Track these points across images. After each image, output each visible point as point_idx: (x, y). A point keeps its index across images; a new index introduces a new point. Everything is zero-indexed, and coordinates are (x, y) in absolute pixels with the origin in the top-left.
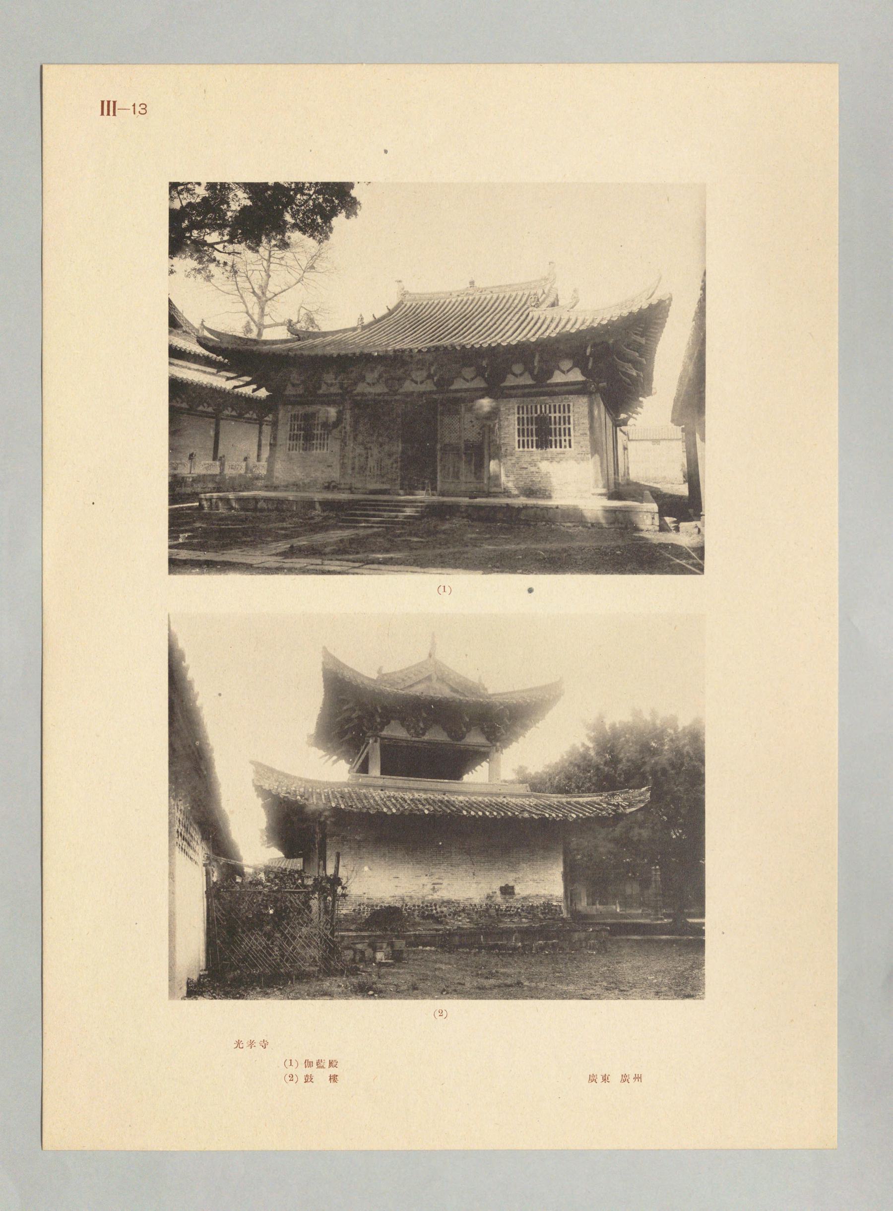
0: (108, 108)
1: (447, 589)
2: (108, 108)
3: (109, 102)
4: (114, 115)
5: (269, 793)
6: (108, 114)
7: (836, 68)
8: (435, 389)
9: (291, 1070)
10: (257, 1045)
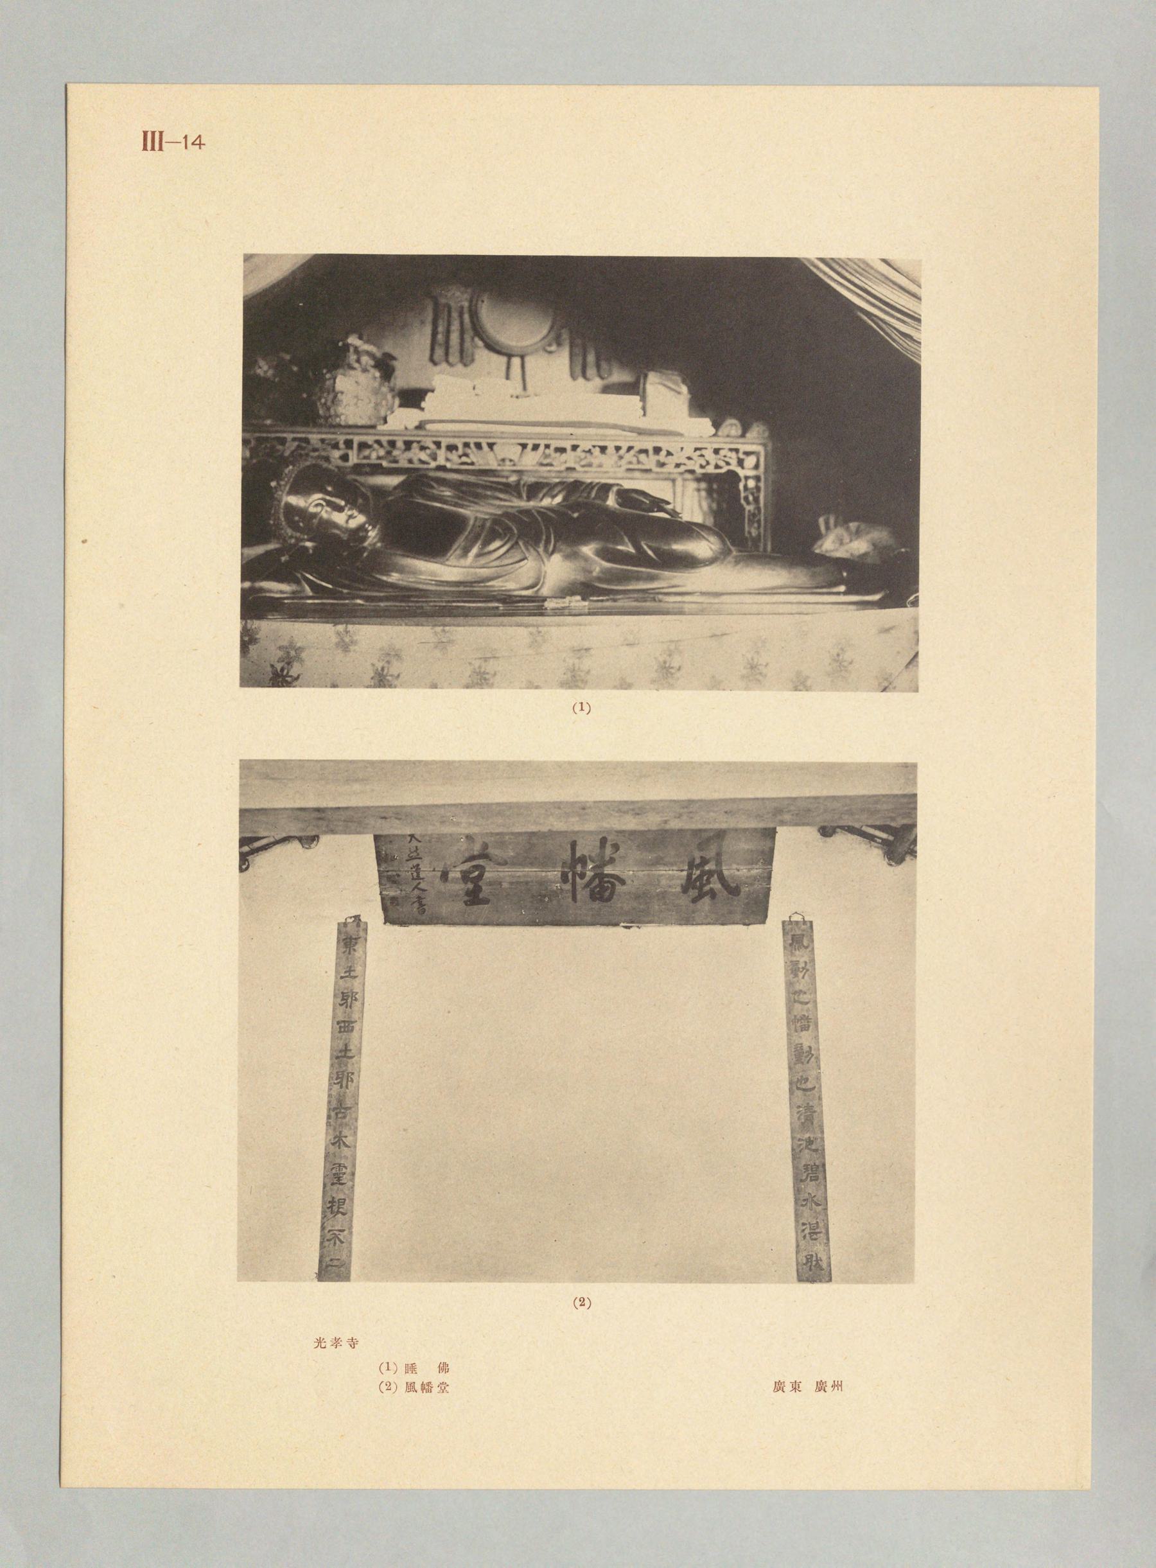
0: (152, 141)
2: (152, 141)
3: (153, 149)
4: (161, 149)
5: (706, 478)
6: (153, 149)
8: (578, 855)
9: (388, 1376)
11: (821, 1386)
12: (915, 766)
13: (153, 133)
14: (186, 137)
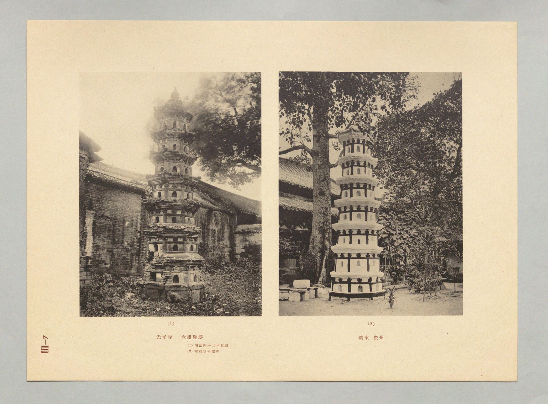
0: (45, 350)
1: (172, 323)
2: (45, 350)
4: (48, 347)
6: (42, 349)
7: (30, 22)
10: (167, 337)
11: (376, 338)
13: (42, 349)
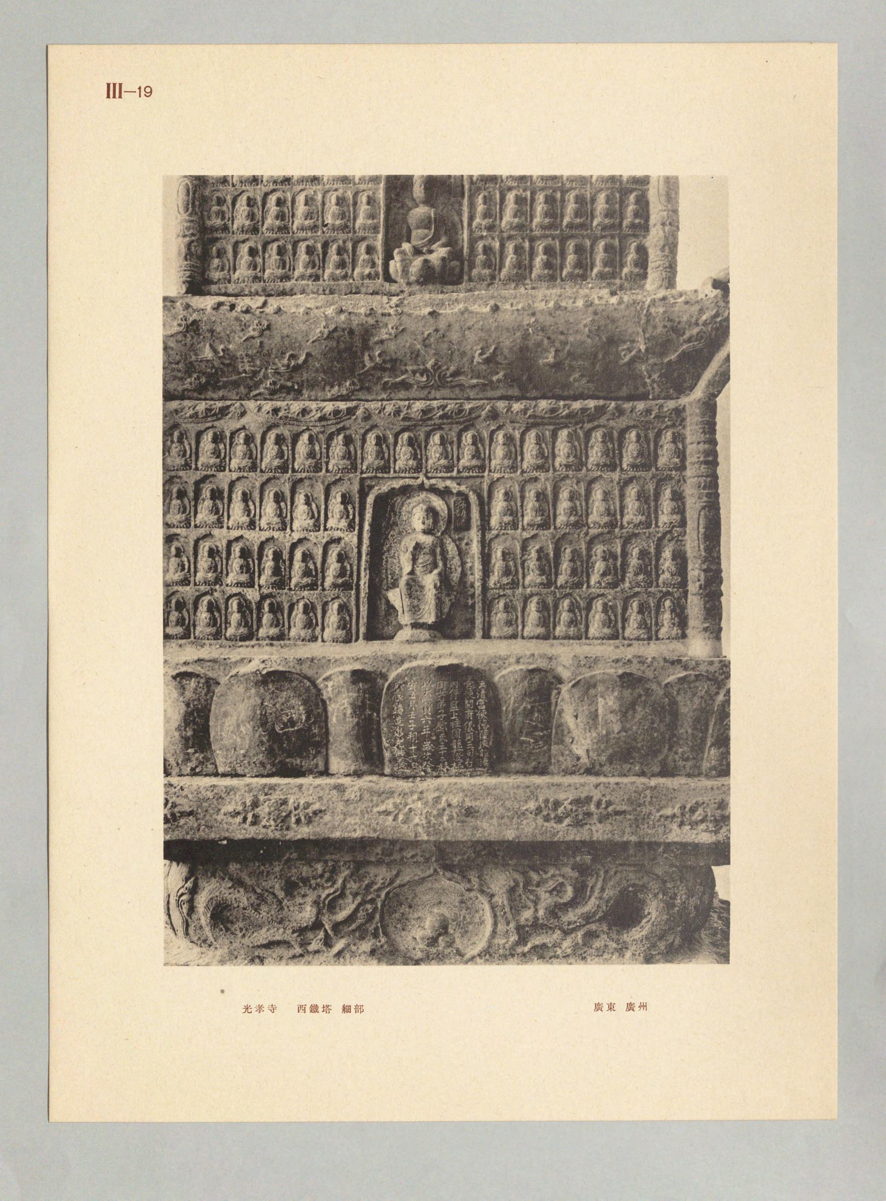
0: (114, 91)
2: (114, 91)
3: (114, 85)
4: (120, 97)
6: (114, 97)
7: (836, 46)
10: (266, 1009)
12: (204, 199)
13: (114, 97)
14: (140, 88)
